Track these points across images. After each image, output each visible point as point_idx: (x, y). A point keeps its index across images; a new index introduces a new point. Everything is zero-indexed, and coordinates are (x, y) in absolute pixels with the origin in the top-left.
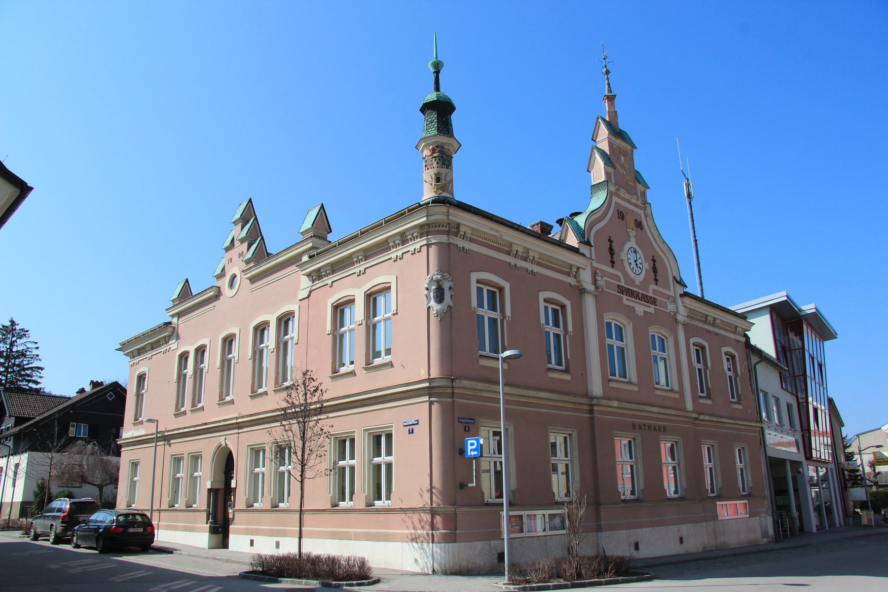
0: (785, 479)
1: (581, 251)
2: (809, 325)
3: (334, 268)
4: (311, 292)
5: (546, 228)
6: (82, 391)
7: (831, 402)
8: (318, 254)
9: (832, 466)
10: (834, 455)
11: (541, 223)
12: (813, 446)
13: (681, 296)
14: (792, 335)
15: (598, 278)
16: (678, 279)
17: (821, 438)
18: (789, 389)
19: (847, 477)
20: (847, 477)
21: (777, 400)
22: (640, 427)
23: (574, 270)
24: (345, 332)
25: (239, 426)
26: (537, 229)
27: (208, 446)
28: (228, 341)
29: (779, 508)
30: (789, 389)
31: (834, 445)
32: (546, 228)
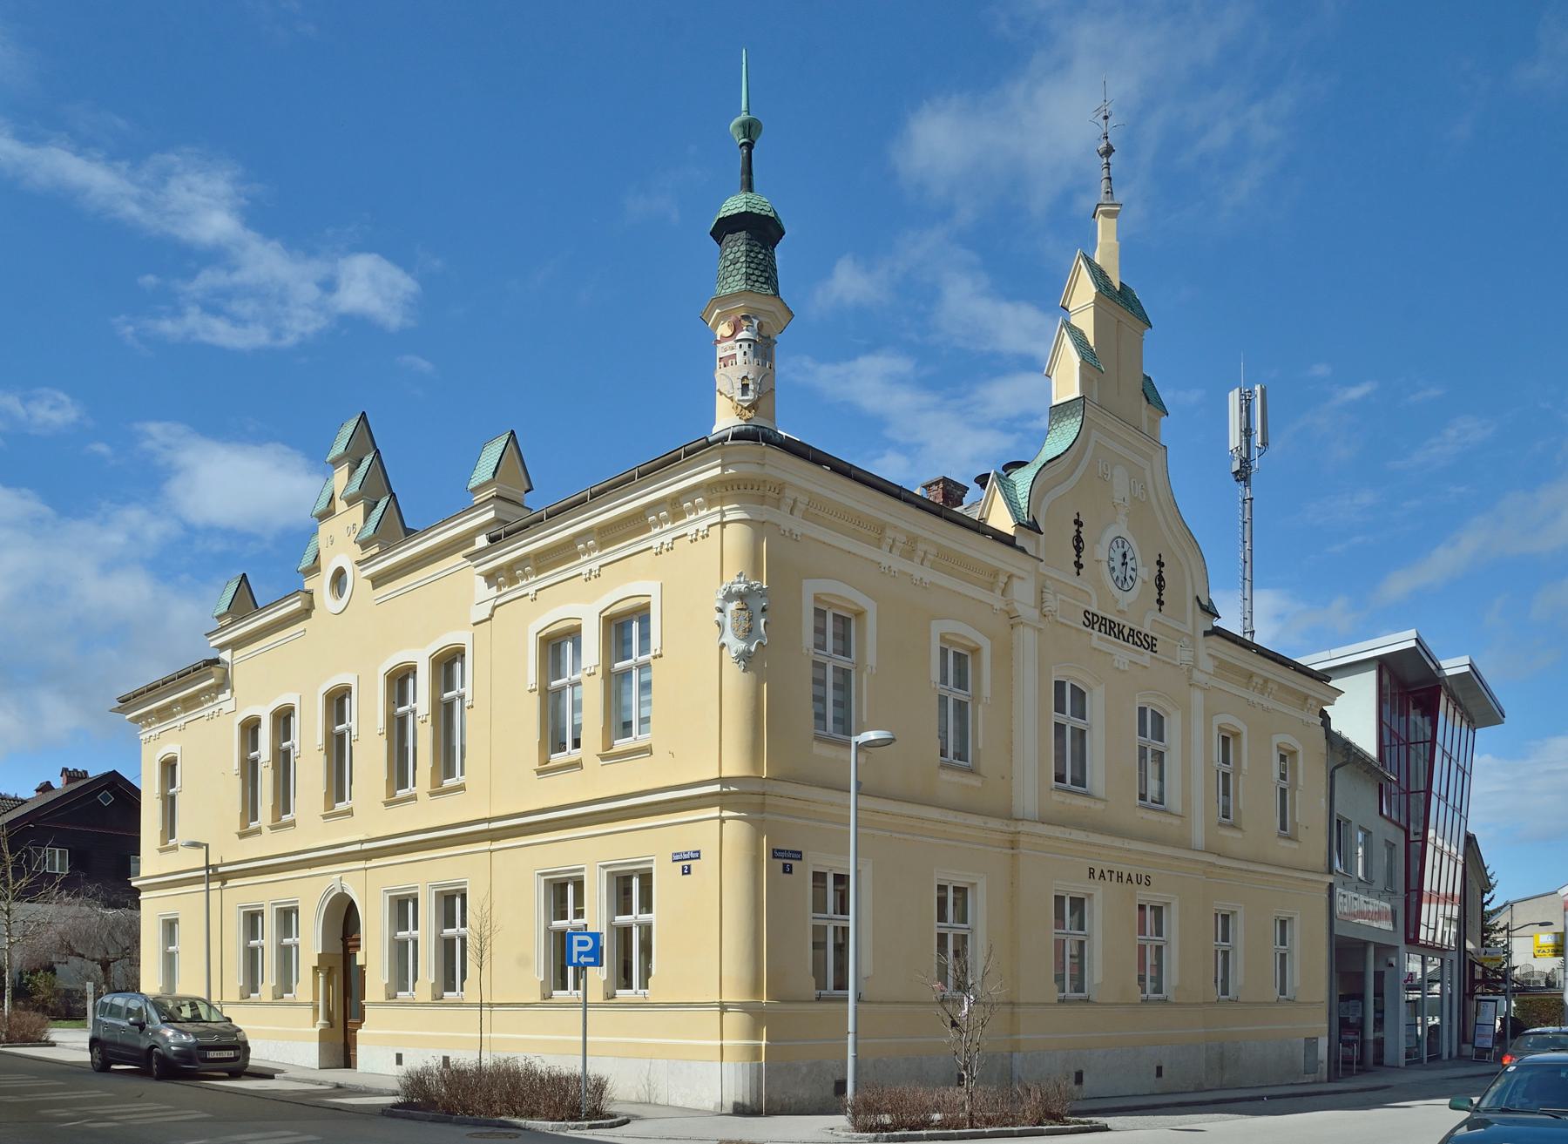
0: (1361, 976)
1: (1018, 543)
2: (1452, 697)
3: (544, 561)
4: (494, 608)
5: (953, 491)
6: (46, 788)
7: (1470, 840)
8: (507, 534)
9: (1455, 956)
10: (1462, 937)
11: (945, 480)
12: (1424, 919)
13: (1206, 634)
14: (1415, 716)
15: (1048, 596)
16: (1205, 602)
17: (1441, 907)
18: (1395, 817)
19: (1478, 976)
20: (1478, 976)
21: (1367, 834)
22: (1102, 875)
23: (1003, 579)
24: (564, 688)
25: (366, 855)
26: (936, 496)
27: (310, 895)
28: (337, 701)
29: (1344, 1024)
30: (1395, 817)
31: (1462, 922)
32: (953, 491)
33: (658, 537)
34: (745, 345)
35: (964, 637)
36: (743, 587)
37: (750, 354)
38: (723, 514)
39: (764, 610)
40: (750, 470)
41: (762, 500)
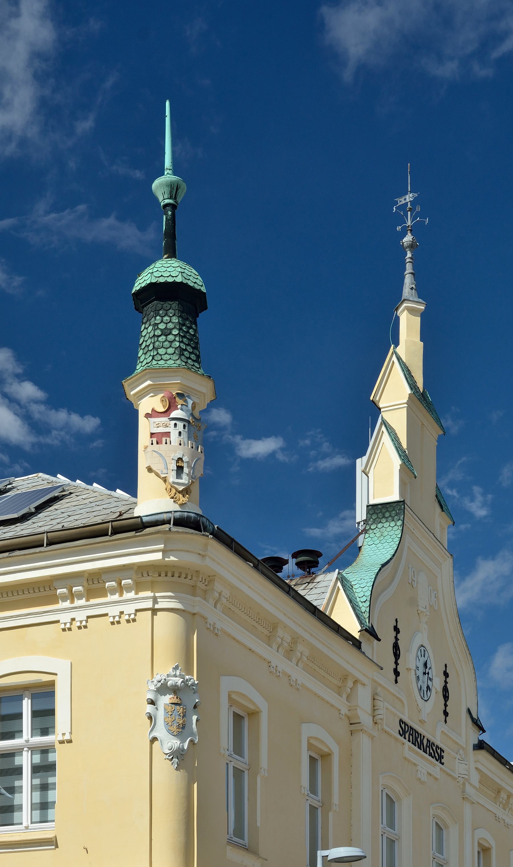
16: (475, 716)
33: (63, 612)
34: (180, 425)
35: (322, 742)
36: (179, 681)
37: (184, 435)
38: (155, 600)
39: (195, 707)
40: (191, 560)
41: (193, 590)
